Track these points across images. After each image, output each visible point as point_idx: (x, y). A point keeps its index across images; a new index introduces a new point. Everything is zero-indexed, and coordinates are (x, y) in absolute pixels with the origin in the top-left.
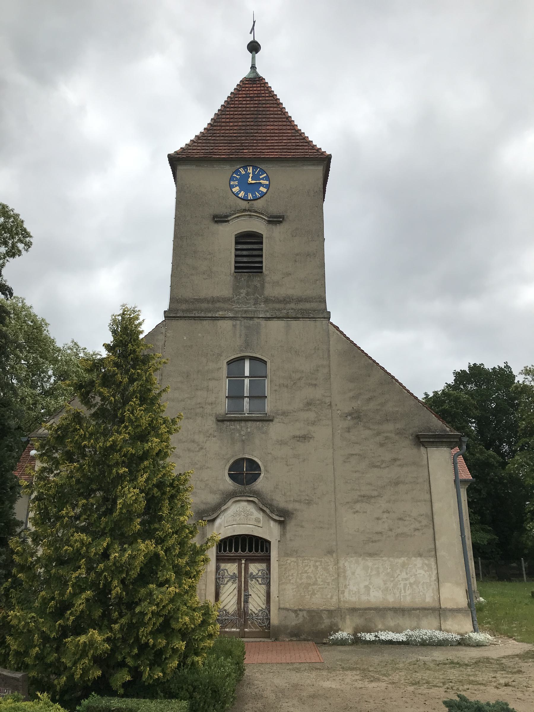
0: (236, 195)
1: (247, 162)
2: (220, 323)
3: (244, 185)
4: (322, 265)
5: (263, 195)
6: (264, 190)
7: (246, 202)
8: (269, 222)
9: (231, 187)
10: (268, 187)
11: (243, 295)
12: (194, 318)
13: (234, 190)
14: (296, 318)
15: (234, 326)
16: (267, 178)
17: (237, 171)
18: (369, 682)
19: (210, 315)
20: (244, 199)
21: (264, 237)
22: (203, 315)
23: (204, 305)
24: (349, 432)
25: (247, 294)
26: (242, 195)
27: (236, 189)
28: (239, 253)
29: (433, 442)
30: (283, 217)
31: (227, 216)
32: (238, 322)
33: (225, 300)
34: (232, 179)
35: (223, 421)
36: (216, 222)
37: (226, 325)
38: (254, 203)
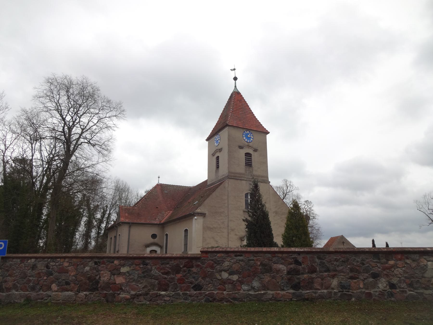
0: (245, 140)
1: (247, 130)
2: (243, 181)
3: (247, 138)
4: (267, 167)
5: (252, 141)
6: (252, 140)
7: (247, 143)
8: (254, 151)
9: (243, 137)
10: (253, 139)
11: (248, 173)
12: (236, 179)
13: (244, 138)
14: (262, 182)
15: (246, 183)
16: (253, 136)
17: (244, 132)
18: (117, 183)
19: (240, 179)
20: (247, 142)
21: (252, 155)
22: (238, 178)
23: (238, 175)
24: (274, 217)
25: (249, 173)
26: (246, 140)
27: (244, 138)
28: (250, 162)
29: (222, 176)
30: (257, 150)
31: (243, 147)
32: (247, 182)
33: (243, 174)
34: (243, 134)
35: (245, 212)
36: (240, 148)
37: (244, 182)
38: (250, 143)
